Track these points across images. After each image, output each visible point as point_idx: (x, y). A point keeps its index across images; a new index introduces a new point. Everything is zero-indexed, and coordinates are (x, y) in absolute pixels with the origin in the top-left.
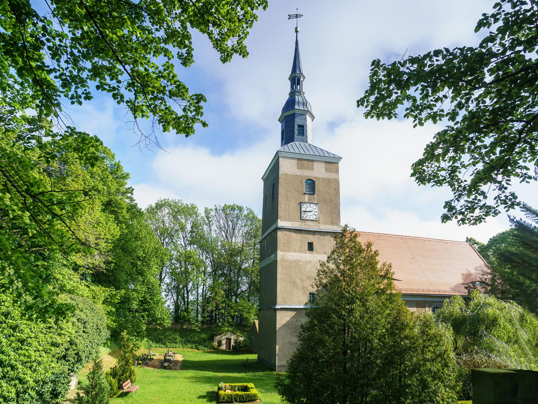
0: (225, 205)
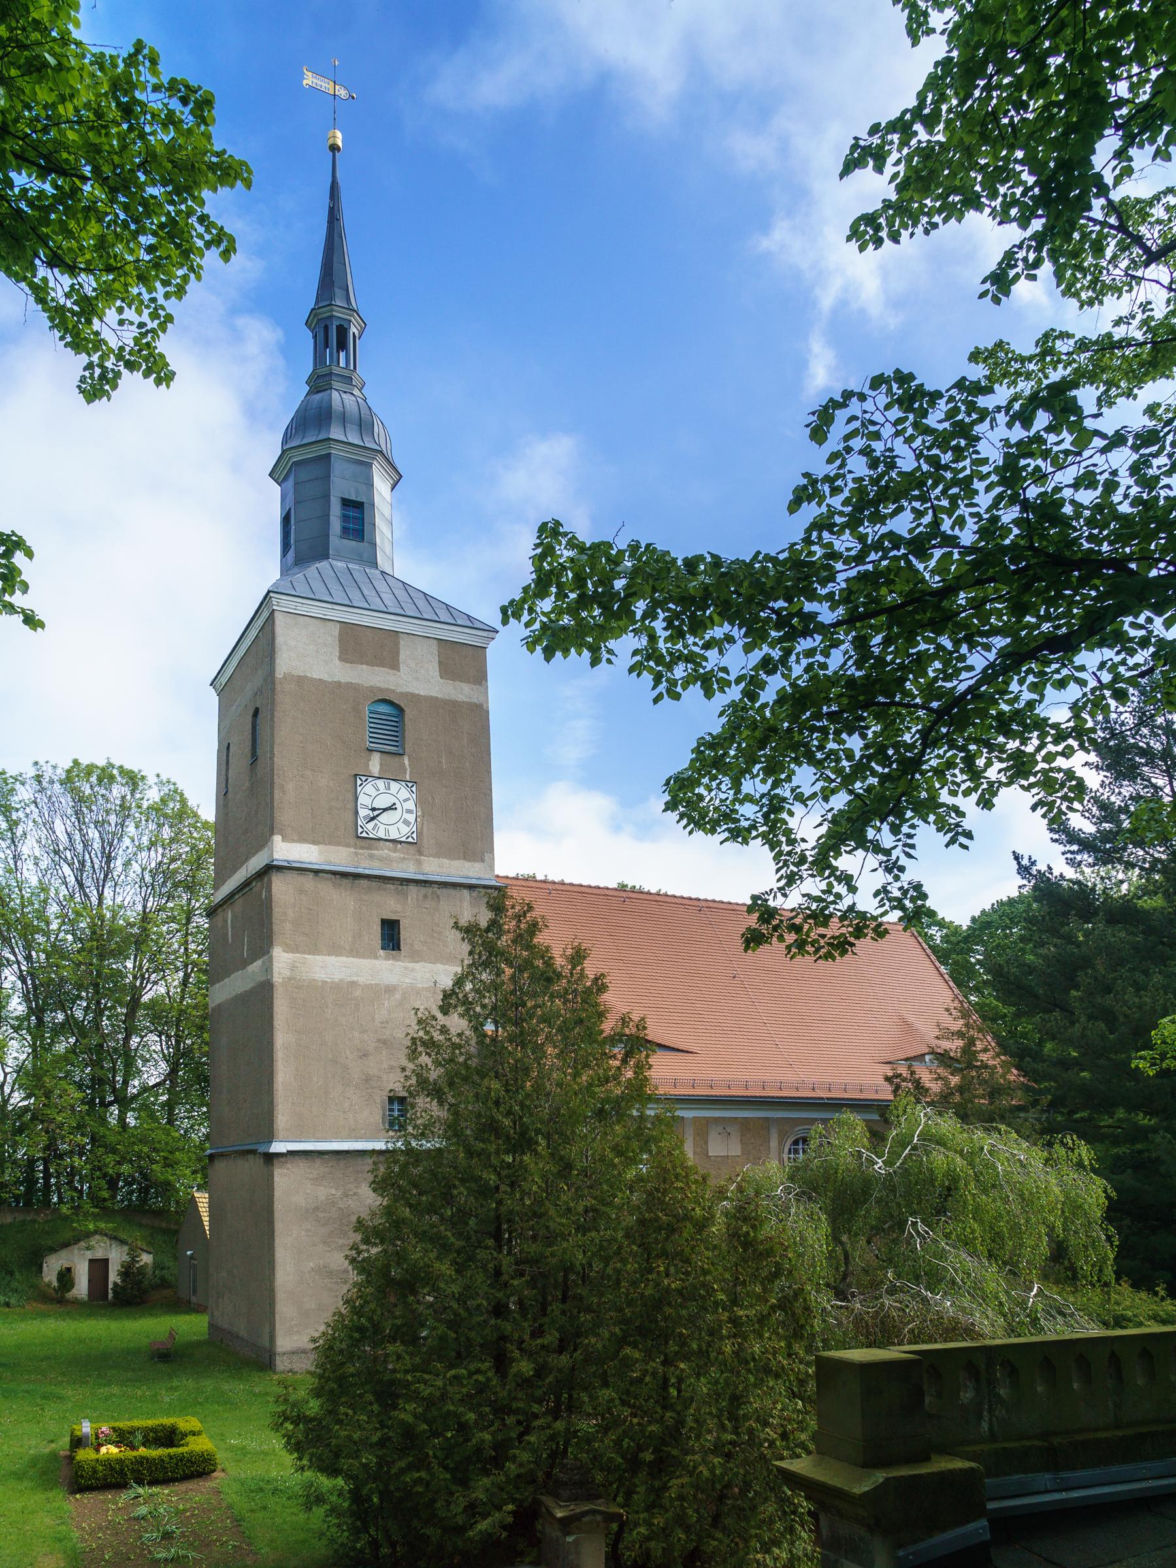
0: (76, 762)
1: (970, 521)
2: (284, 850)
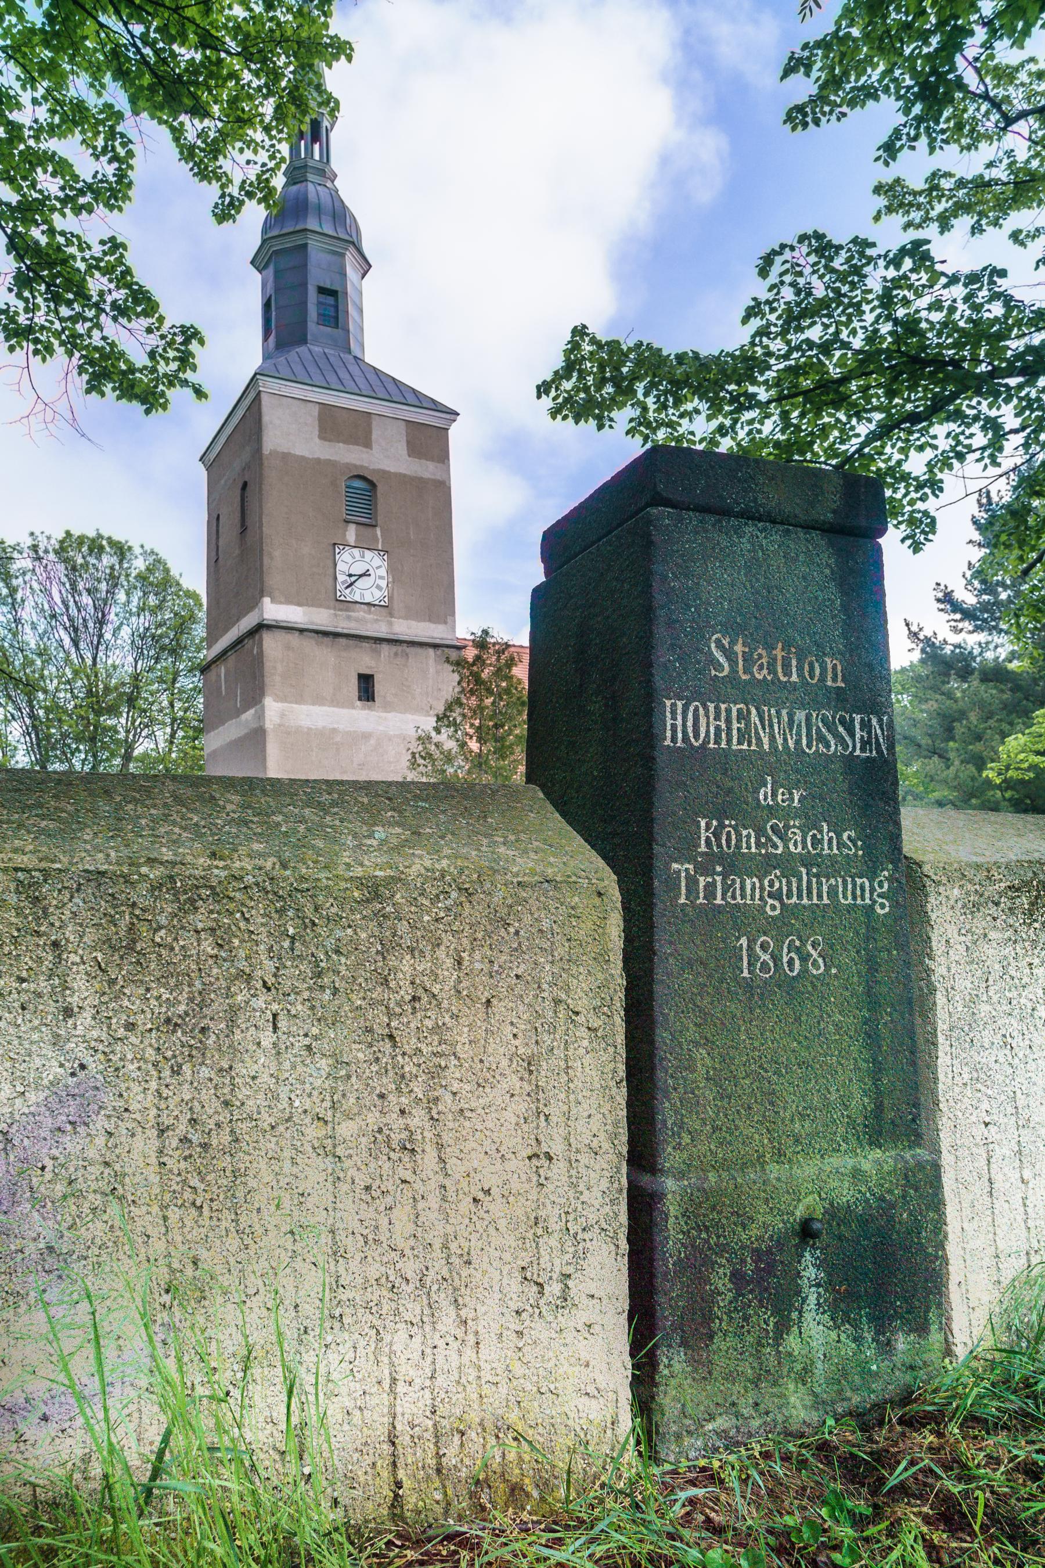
1: (860, 331)
2: (272, 610)
